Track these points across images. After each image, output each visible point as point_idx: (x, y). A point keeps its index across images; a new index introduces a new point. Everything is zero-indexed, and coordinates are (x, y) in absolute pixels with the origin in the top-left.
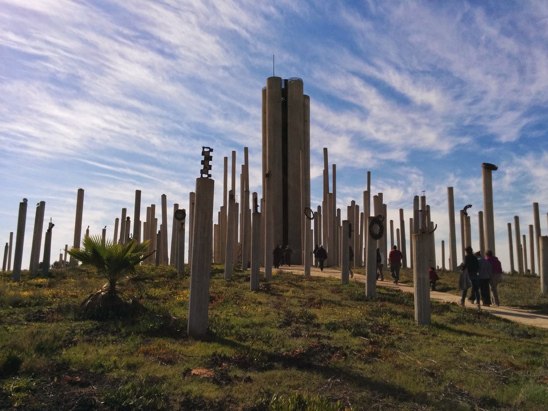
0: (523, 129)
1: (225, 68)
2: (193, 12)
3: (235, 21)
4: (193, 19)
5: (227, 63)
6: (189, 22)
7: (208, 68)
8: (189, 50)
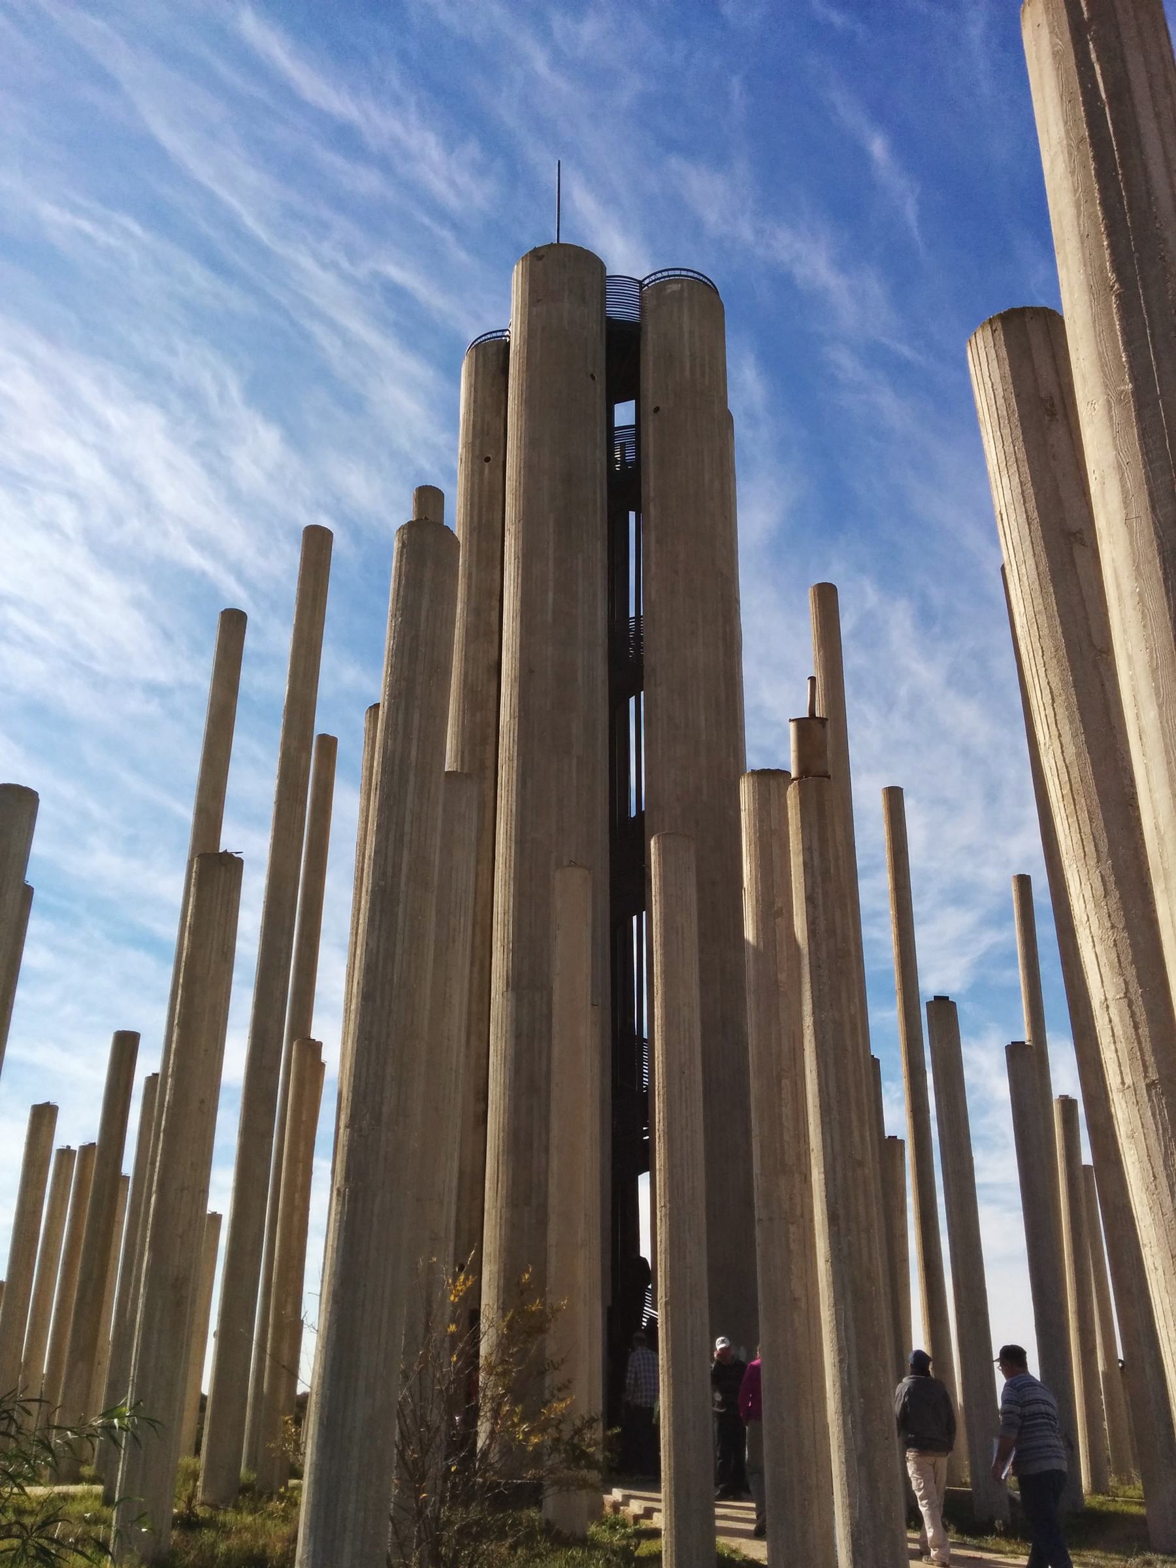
0: (980, 963)
1: (153, 690)
2: (73, 495)
3: (205, 543)
4: (68, 516)
5: (162, 675)
6: (50, 527)
7: (99, 683)
8: (41, 615)
